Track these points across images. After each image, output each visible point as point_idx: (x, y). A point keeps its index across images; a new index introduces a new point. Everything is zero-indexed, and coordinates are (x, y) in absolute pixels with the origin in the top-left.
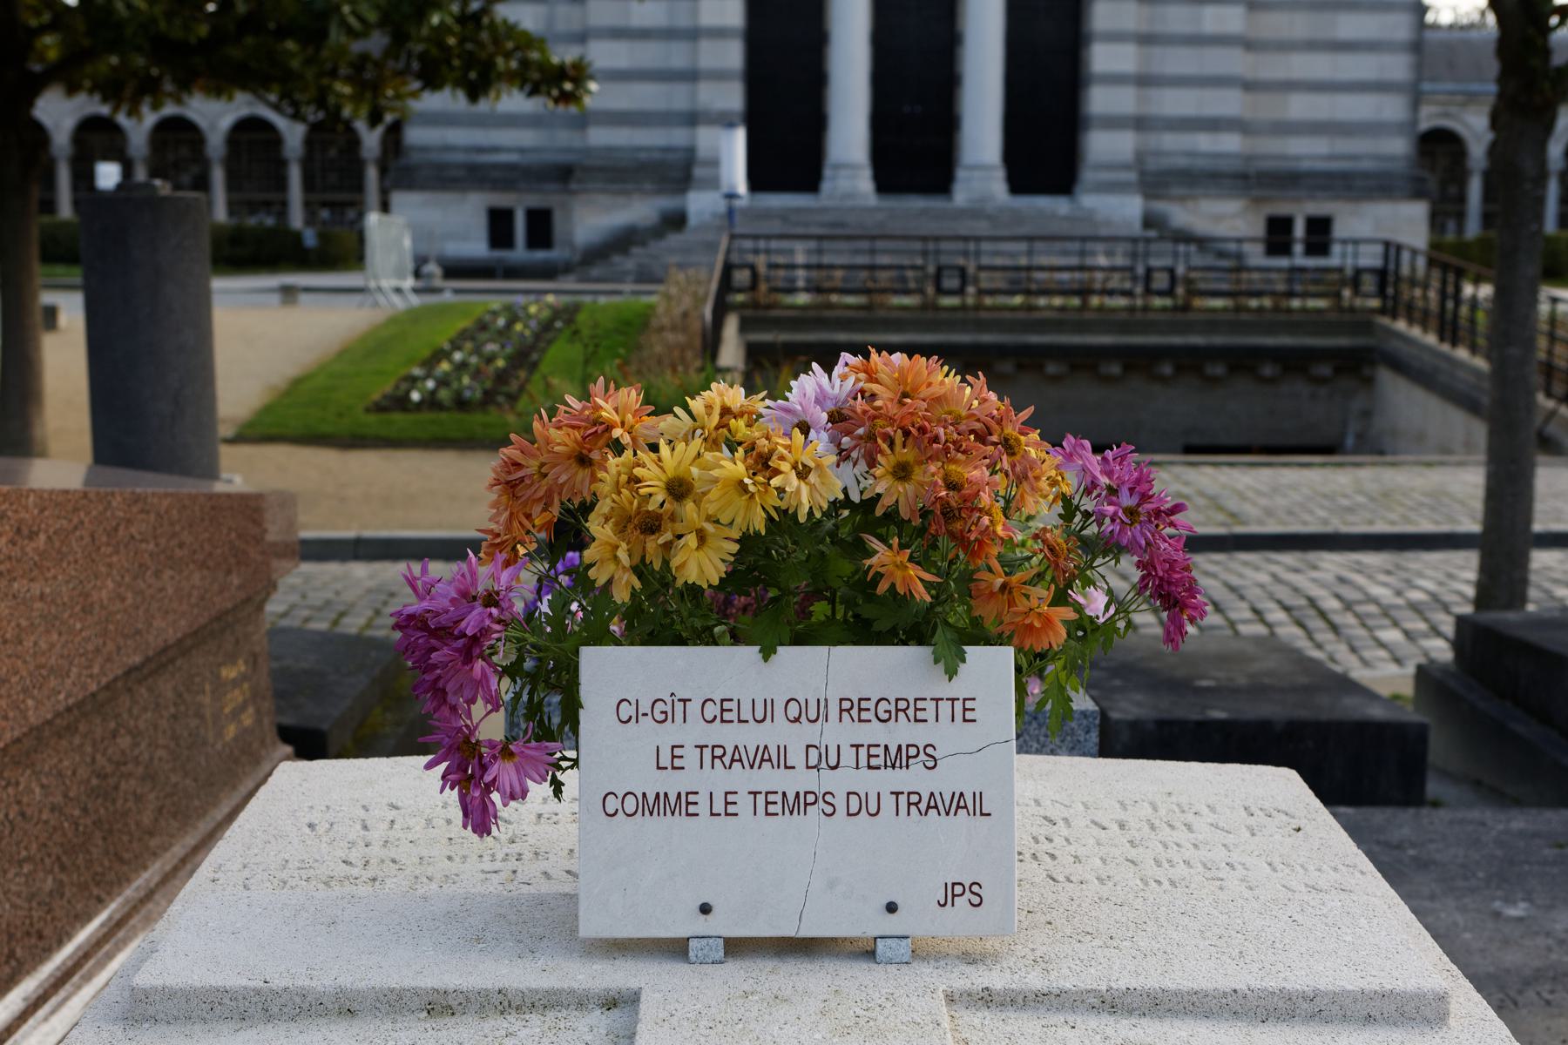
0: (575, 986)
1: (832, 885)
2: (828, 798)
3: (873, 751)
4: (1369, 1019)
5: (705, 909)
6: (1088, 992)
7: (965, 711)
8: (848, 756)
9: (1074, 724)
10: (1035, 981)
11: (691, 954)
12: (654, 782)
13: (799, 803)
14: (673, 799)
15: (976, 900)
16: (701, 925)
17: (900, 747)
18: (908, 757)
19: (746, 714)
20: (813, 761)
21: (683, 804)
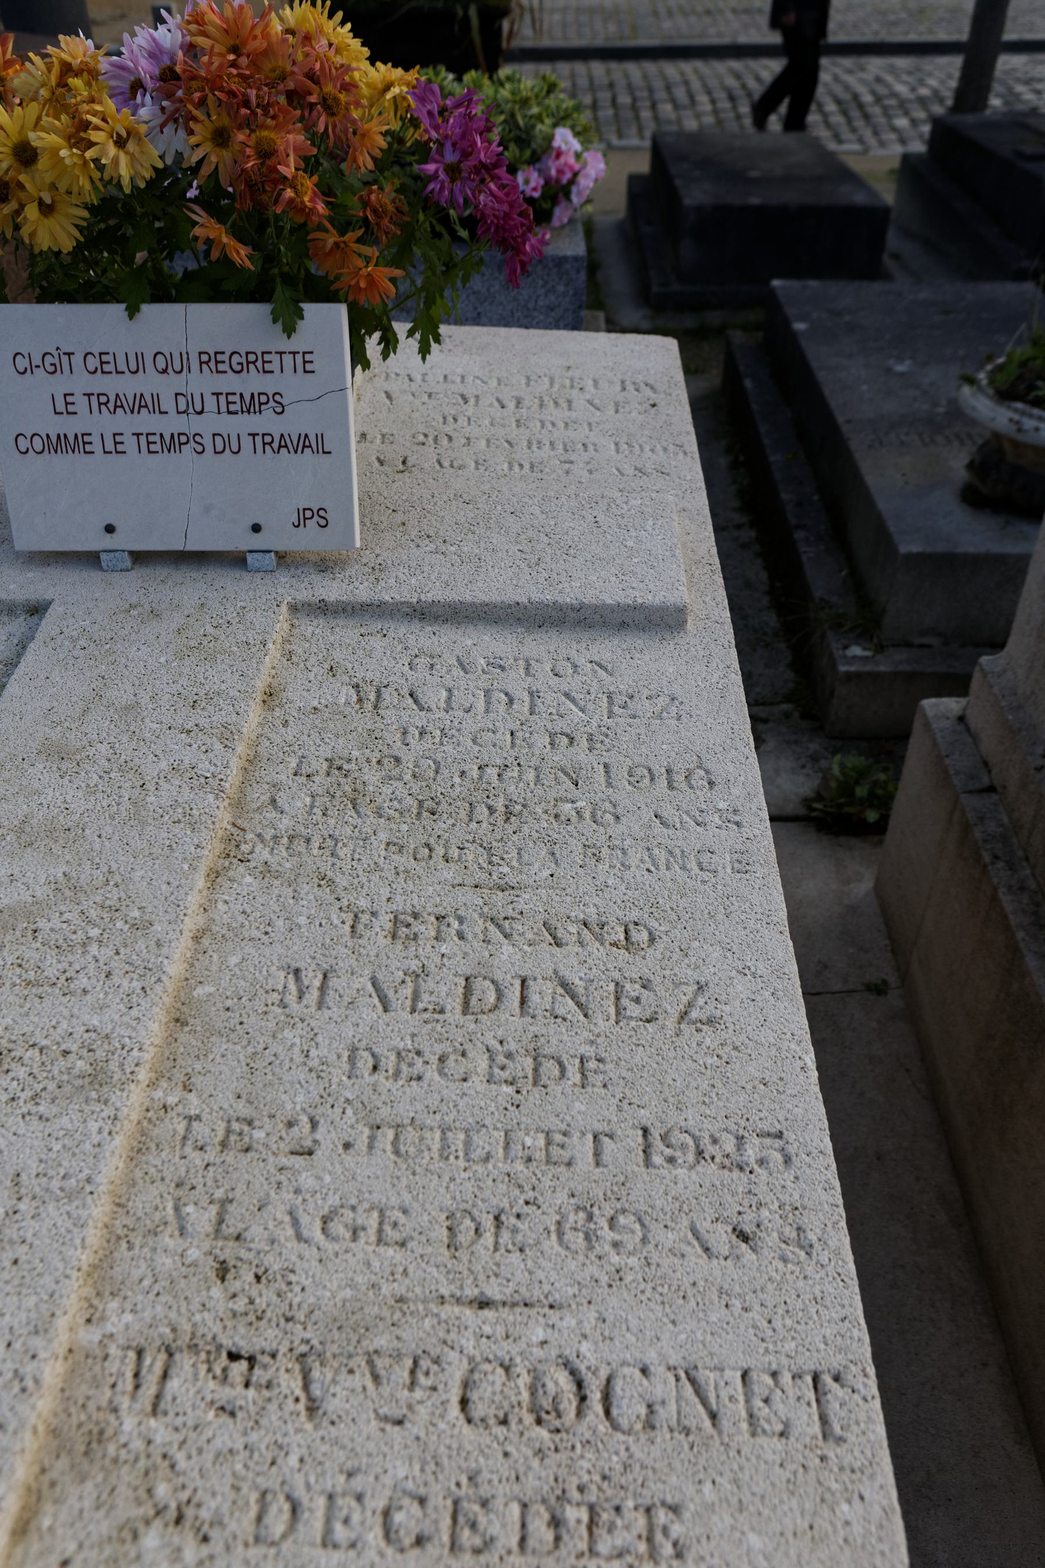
1: (208, 509)
2: (198, 438)
3: (231, 398)
4: (623, 625)
5: (110, 529)
6: (402, 603)
7: (305, 364)
8: (210, 403)
9: (568, 266)
10: (363, 592)
12: (55, 426)
13: (174, 443)
14: (71, 439)
15: (323, 522)
16: (107, 542)
17: (252, 395)
18: (260, 404)
19: (122, 367)
20: (182, 407)
21: (79, 444)
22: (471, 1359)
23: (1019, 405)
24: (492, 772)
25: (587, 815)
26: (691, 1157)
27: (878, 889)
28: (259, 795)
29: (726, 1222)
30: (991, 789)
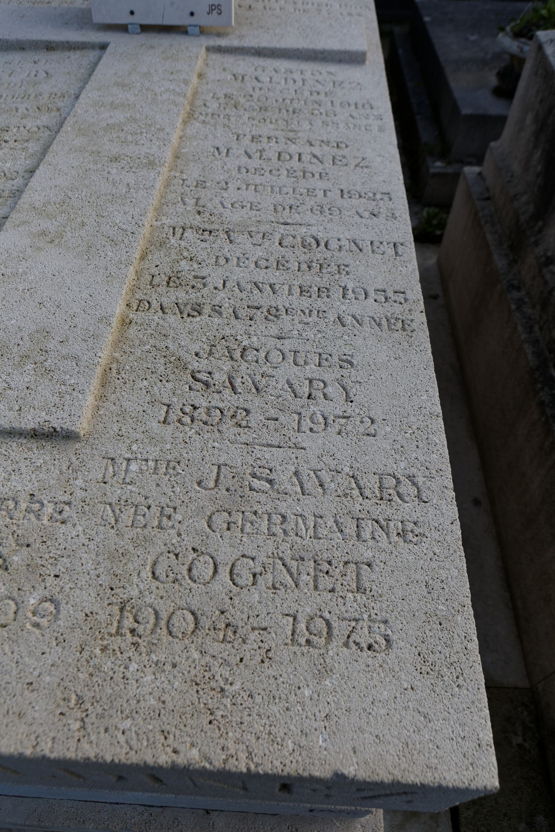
0: (90, 40)
10: (236, 43)
11: (129, 30)
22: (282, 234)
23: (523, 40)
24: (288, 101)
25: (324, 114)
26: (357, 196)
27: (439, 263)
28: (199, 102)
29: (368, 211)
30: (488, 199)
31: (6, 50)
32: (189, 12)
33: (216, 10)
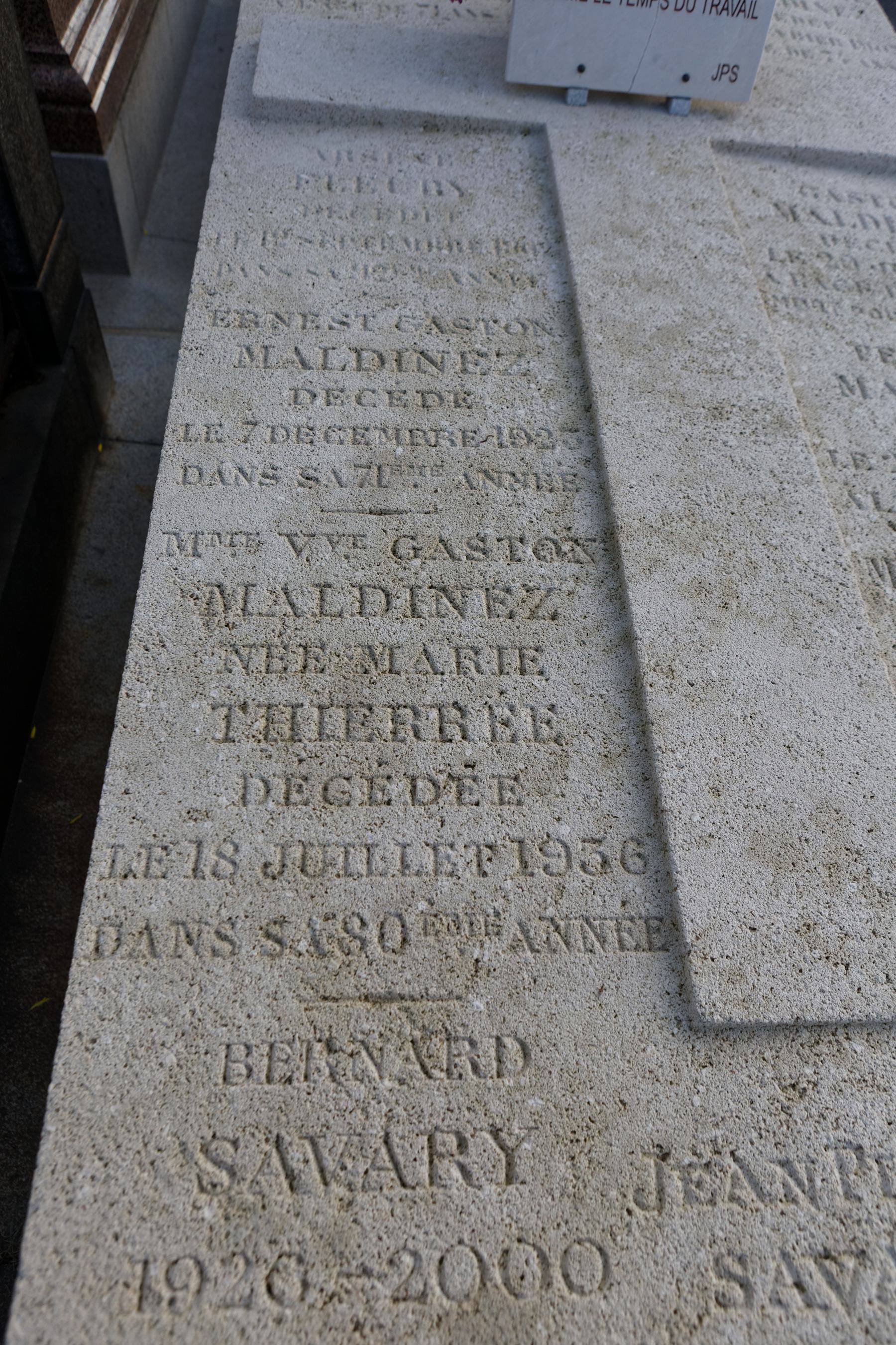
0: (508, 118)
10: (756, 137)
11: (569, 99)
31: (347, 125)
32: (682, 74)
33: (730, 73)
